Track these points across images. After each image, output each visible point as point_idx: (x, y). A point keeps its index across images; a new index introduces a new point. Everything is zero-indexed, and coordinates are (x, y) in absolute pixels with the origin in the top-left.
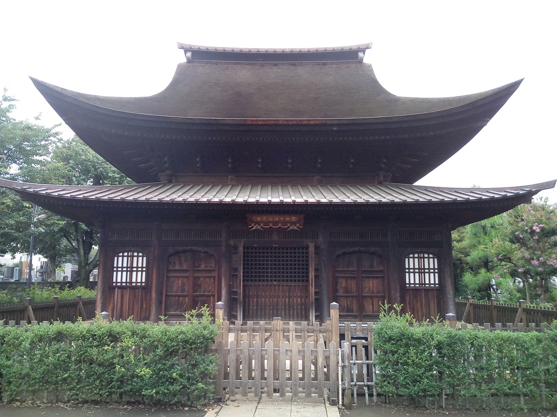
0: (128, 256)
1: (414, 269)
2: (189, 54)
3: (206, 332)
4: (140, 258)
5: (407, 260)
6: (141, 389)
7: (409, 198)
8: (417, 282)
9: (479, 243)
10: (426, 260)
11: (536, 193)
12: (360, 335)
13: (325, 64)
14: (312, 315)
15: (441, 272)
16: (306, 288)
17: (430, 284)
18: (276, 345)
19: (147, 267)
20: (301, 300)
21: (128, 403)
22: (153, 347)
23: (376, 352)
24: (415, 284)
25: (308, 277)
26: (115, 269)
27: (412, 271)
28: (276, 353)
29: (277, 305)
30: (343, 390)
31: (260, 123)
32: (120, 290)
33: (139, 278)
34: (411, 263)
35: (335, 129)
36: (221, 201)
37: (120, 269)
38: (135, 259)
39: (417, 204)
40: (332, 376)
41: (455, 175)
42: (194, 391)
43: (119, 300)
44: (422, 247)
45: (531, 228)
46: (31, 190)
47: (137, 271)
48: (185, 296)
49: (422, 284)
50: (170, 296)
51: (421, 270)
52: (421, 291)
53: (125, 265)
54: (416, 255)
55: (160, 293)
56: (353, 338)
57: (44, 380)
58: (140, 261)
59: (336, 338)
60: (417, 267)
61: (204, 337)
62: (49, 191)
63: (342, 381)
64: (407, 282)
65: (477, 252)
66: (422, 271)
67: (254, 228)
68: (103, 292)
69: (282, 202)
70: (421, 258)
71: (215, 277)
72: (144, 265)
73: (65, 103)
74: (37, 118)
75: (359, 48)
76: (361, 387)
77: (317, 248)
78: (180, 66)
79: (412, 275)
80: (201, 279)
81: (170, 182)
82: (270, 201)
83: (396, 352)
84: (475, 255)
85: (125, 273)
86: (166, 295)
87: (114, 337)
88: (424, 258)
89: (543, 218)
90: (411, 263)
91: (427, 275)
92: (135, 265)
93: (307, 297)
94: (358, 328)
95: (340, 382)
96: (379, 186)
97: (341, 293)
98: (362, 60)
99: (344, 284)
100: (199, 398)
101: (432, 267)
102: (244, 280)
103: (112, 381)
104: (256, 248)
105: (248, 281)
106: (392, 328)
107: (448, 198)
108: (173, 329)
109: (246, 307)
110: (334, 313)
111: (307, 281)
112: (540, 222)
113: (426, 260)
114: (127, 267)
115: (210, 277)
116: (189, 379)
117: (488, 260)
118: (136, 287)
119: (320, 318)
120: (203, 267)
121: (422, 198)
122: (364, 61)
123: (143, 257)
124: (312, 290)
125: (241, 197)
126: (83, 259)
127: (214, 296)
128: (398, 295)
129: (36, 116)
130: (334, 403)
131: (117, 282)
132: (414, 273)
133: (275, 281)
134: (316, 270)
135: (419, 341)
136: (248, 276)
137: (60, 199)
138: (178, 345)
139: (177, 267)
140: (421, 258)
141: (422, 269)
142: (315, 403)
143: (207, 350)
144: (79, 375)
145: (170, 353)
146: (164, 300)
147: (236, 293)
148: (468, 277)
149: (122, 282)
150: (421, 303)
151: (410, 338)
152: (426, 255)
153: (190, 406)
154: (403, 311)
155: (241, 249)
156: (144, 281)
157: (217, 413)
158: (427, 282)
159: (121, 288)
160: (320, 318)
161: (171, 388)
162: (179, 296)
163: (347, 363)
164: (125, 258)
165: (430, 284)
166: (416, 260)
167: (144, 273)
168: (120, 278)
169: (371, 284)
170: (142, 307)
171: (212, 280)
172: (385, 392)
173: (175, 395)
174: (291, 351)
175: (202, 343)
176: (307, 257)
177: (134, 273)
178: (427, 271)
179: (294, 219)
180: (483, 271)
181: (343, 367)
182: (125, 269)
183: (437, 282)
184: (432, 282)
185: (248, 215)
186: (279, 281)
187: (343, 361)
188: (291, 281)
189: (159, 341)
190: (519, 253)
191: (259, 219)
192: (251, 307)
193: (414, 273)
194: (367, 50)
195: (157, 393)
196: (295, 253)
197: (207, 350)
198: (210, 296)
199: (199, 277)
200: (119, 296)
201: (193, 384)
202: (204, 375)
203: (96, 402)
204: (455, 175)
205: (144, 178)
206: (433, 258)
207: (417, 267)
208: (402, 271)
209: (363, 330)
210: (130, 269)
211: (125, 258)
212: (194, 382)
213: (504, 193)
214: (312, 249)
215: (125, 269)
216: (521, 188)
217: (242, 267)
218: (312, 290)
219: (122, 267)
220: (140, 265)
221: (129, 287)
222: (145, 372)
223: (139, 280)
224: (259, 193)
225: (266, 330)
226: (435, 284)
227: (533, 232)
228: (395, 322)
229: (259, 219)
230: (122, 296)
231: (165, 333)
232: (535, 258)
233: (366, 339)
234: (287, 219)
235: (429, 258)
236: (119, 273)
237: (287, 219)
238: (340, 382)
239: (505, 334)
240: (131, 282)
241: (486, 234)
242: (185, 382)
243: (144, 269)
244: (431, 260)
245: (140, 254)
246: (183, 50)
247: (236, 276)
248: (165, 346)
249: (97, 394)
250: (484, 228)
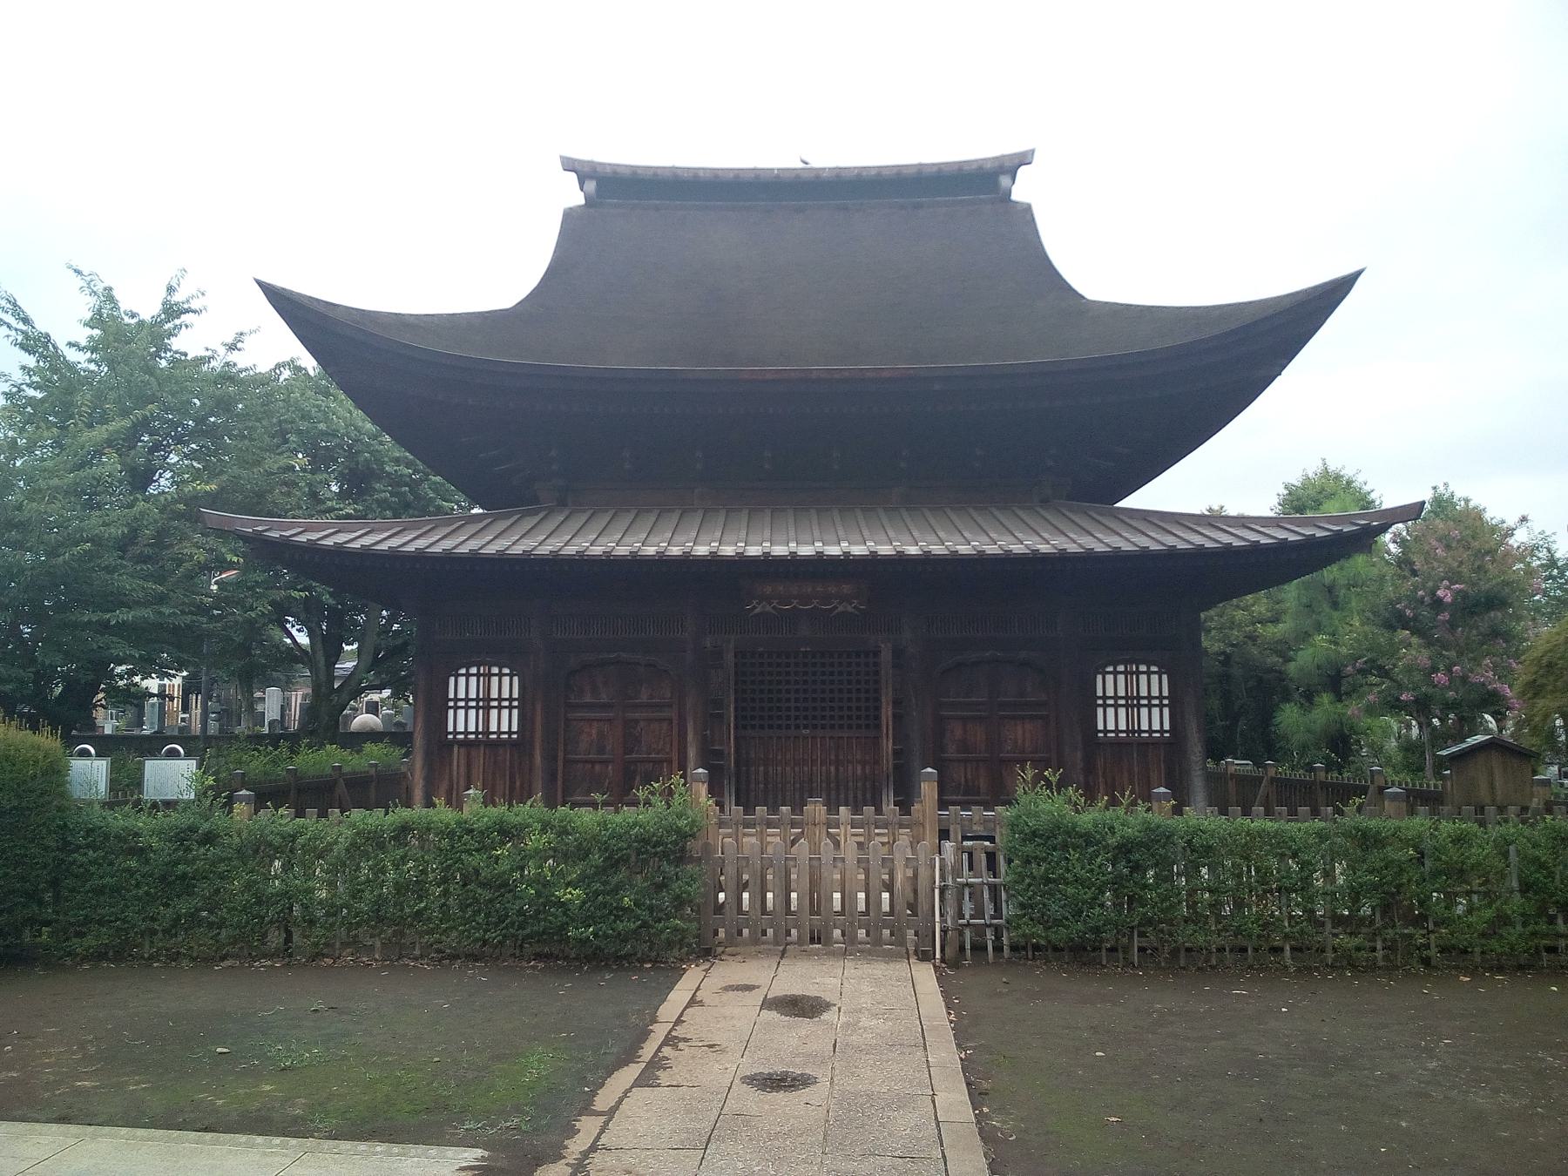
1: (1116, 697)
2: (591, 186)
3: (682, 823)
4: (506, 680)
5: (1099, 678)
6: (563, 928)
8: (1123, 727)
9: (1319, 628)
10: (1143, 678)
11: (1384, 529)
12: (978, 829)
13: (918, 206)
14: (890, 807)
15: (1175, 702)
16: (876, 741)
17: (1151, 731)
18: (815, 848)
19: (521, 699)
20: (863, 769)
21: (538, 956)
22: (582, 853)
23: (1009, 861)
24: (1117, 731)
25: (877, 718)
26: (451, 704)
27: (1156, 702)
28: (815, 863)
29: (811, 781)
30: (944, 931)
31: (769, 376)
32: (462, 750)
33: (505, 722)
34: (1110, 684)
35: (937, 387)
36: (686, 555)
37: (462, 704)
38: (495, 680)
39: (1116, 558)
40: (923, 906)
41: (1227, 479)
42: (662, 932)
43: (463, 770)
44: (1131, 650)
45: (1433, 593)
46: (275, 534)
47: (500, 708)
48: (605, 762)
49: (1134, 732)
50: (577, 762)
51: (1132, 703)
52: (1132, 746)
53: (473, 695)
54: (1121, 668)
55: (550, 757)
56: (965, 838)
57: (378, 917)
58: (506, 686)
59: (930, 838)
60: (1122, 693)
61: (678, 831)
62: (314, 536)
63: (941, 915)
64: (1100, 727)
65: (1311, 650)
66: (1133, 702)
67: (757, 611)
68: (428, 754)
69: (820, 554)
70: (1132, 673)
71: (670, 721)
72: (516, 695)
73: (293, 309)
74: (232, 347)
76: (979, 931)
77: (898, 653)
78: (569, 215)
79: (1111, 711)
80: (642, 724)
81: (562, 503)
82: (793, 554)
83: (1044, 860)
84: (1305, 659)
85: (472, 713)
86: (566, 762)
87: (507, 832)
88: (1138, 673)
89: (1464, 569)
90: (1110, 684)
91: (1144, 711)
92: (494, 694)
93: (876, 762)
94: (976, 818)
95: (937, 918)
96: (1043, 512)
97: (951, 752)
99: (958, 733)
100: (670, 945)
101: (1155, 693)
102: (736, 727)
103: (507, 916)
104: (761, 655)
105: (745, 727)
106: (1036, 815)
108: (619, 819)
109: (746, 786)
110: (928, 790)
111: (878, 727)
112: (1454, 577)
113: (1143, 678)
114: (477, 700)
115: (661, 720)
116: (651, 909)
117: (1339, 671)
118: (499, 743)
119: (905, 805)
120: (644, 698)
122: (1014, 197)
123: (511, 676)
124: (888, 746)
125: (729, 544)
126: (323, 677)
127: (670, 762)
128: (1079, 754)
129: (230, 340)
130: (925, 957)
131: (455, 733)
132: (1116, 706)
133: (806, 727)
134: (896, 703)
135: (1088, 839)
136: (745, 718)
137: (312, 548)
138: (629, 847)
139: (588, 699)
140: (1132, 673)
141: (1133, 698)
142: (890, 957)
143: (681, 857)
144: (444, 905)
145: (614, 862)
146: (560, 768)
147: (719, 754)
148: (1289, 716)
149: (466, 733)
150: (1108, 766)
151: (1071, 831)
152: (1143, 668)
153: (655, 962)
154: (1062, 784)
155: (730, 658)
156: (515, 728)
157: (707, 970)
158: (1145, 727)
159: (466, 743)
160: (905, 805)
161: (620, 926)
162: (593, 762)
163: (950, 882)
164: (473, 680)
165: (1151, 731)
166: (1121, 678)
167: (515, 712)
168: (462, 722)
169: (1020, 732)
170: (512, 783)
171: (665, 725)
172: (1024, 935)
173: (625, 941)
174: (843, 860)
175: (675, 843)
176: (876, 682)
177: (494, 713)
178: (495, 704)
179: (846, 589)
180: (1325, 698)
181: (943, 891)
182: (473, 704)
183: (1167, 727)
184: (1156, 727)
186: (815, 727)
187: (943, 878)
188: (841, 727)
189: (594, 837)
190: (1412, 653)
192: (752, 786)
193: (1116, 706)
194: (1022, 171)
195: (595, 935)
196: (858, 700)
197: (681, 857)
198: (661, 761)
199: (637, 721)
200: (463, 762)
201: (659, 921)
202: (680, 902)
203: (474, 957)
204: (1227, 479)
205: (505, 496)
206: (1160, 674)
207: (1122, 693)
208: (1088, 703)
209: (986, 821)
210: (484, 704)
211: (473, 680)
212: (661, 915)
213: (1308, 532)
214: (886, 656)
215: (506, 703)
217: (732, 698)
218: (888, 746)
219: (467, 700)
221: (484, 743)
222: (574, 895)
223: (505, 728)
224: (767, 533)
225: (793, 825)
226: (1162, 731)
227: (1438, 604)
228: (1044, 803)
230: (469, 765)
231: (604, 824)
232: (1441, 667)
233: (992, 839)
234: (832, 589)
235: (1149, 673)
236: (461, 713)
237: (832, 589)
238: (937, 918)
239: (1269, 825)
240: (487, 732)
241: (1335, 605)
242: (645, 915)
243: (1166, 702)
244: (1155, 678)
245: (506, 671)
246: (573, 176)
247: (720, 716)
248: (606, 850)
249: (477, 940)
250: (1330, 589)
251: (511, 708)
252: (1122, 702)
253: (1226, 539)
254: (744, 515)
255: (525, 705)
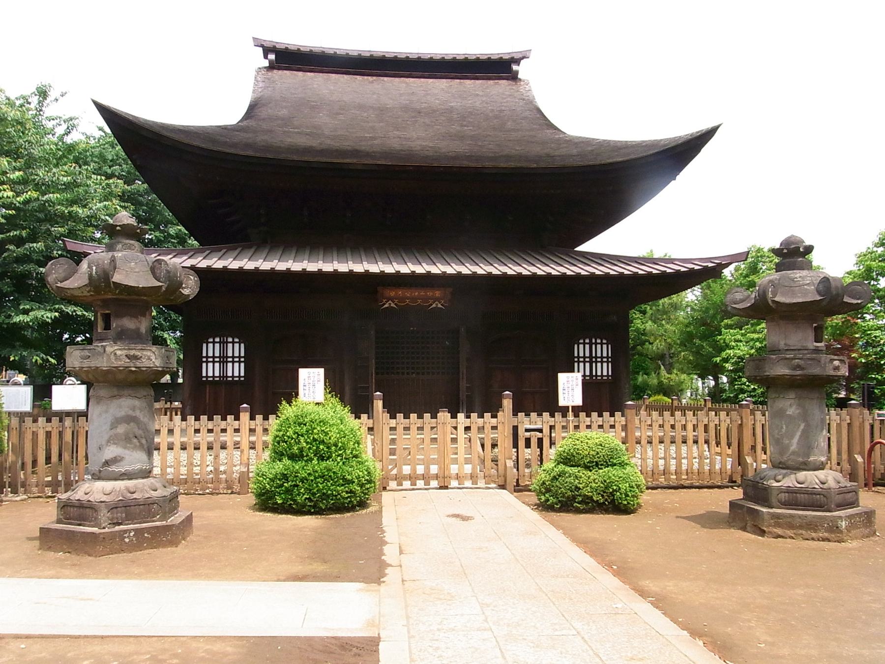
0: (220, 342)
2: (272, 57)
4: (237, 345)
7: (569, 270)
24: (214, 377)
27: (211, 360)
37: (599, 360)
38: (230, 345)
41: (635, 238)
47: (233, 362)
67: (386, 306)
75: (513, 58)
98: (517, 72)
102: (377, 374)
107: (628, 270)
121: (584, 270)
132: (214, 362)
152: (230, 340)
158: (230, 374)
165: (233, 377)
166: (217, 345)
168: (211, 370)
178: (230, 359)
179: (438, 294)
184: (236, 374)
185: (379, 289)
186: (418, 373)
191: (393, 294)
193: (214, 362)
204: (635, 238)
205: (212, 237)
206: (240, 343)
210: (223, 360)
213: (691, 266)
215: (237, 359)
216: (709, 260)
219: (214, 357)
220: (236, 354)
223: (236, 374)
229: (393, 294)
237: (430, 294)
243: (242, 360)
244: (605, 346)
251: (240, 362)
252: (217, 360)
253: (607, 271)
254: (307, 252)
255: (248, 360)
